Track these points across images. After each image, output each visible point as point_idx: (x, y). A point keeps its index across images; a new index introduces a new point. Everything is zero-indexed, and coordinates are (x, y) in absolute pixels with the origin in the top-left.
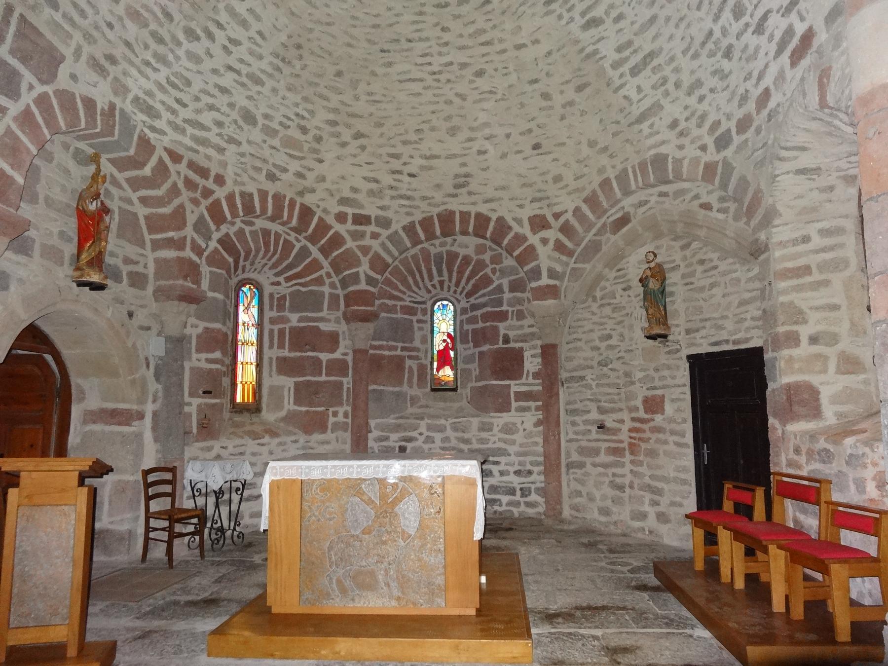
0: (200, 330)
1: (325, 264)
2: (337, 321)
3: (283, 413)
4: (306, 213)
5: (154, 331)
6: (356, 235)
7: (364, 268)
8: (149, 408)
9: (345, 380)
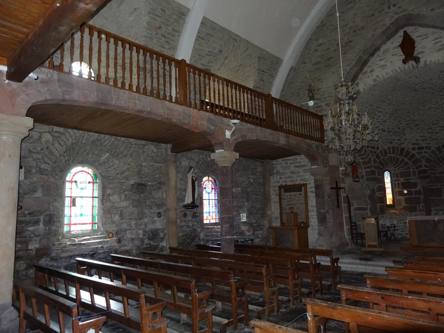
0: (377, 186)
1: (410, 162)
2: (416, 179)
3: (402, 207)
4: (403, 149)
5: (367, 188)
6: (419, 153)
7: (423, 163)
8: (369, 207)
9: (421, 196)
